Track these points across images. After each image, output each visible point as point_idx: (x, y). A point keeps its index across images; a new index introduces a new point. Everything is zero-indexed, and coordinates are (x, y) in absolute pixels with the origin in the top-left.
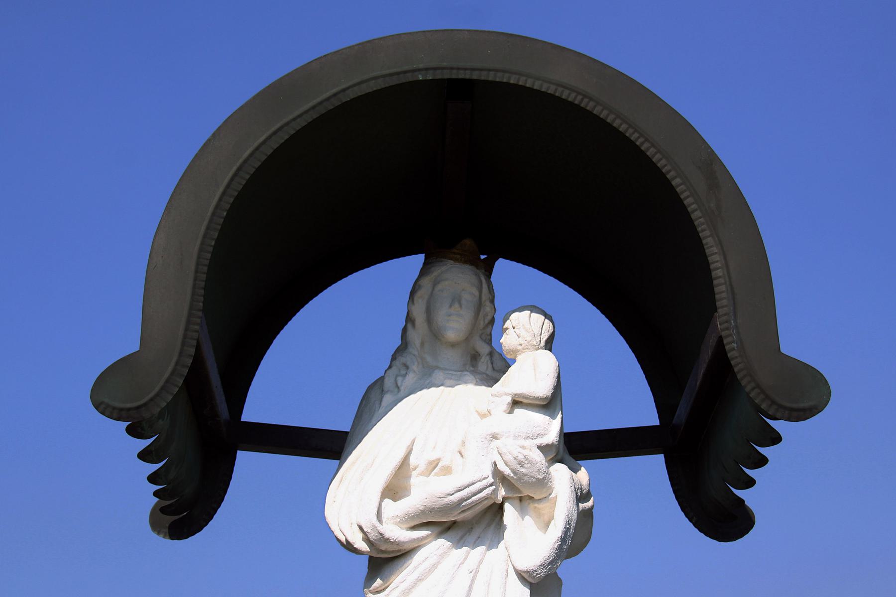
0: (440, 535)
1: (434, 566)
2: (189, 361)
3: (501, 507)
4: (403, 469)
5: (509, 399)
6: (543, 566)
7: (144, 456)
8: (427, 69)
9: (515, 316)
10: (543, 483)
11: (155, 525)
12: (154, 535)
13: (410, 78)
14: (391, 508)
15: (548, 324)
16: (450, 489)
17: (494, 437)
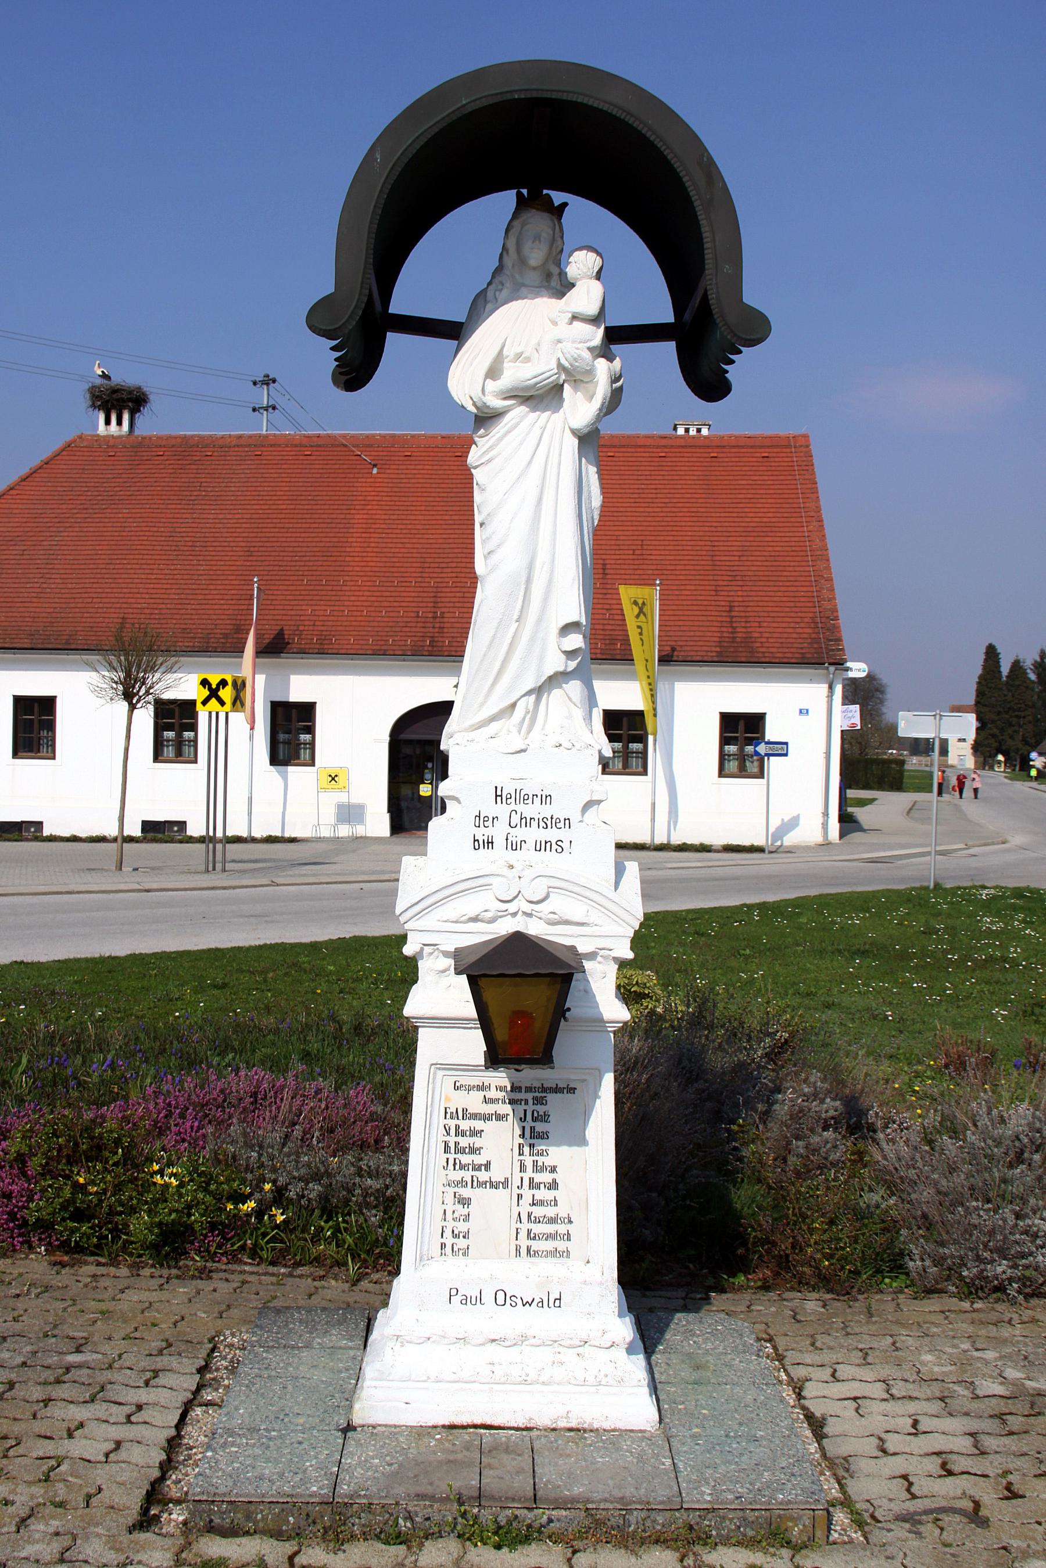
0: (521, 404)
1: (518, 424)
2: (366, 299)
3: (562, 385)
4: (499, 358)
5: (570, 315)
6: (587, 426)
7: (333, 349)
8: (521, 90)
9: (576, 254)
10: (590, 372)
11: (336, 382)
12: (335, 388)
13: (509, 97)
14: (492, 386)
15: (599, 260)
16: (529, 376)
17: (559, 341)
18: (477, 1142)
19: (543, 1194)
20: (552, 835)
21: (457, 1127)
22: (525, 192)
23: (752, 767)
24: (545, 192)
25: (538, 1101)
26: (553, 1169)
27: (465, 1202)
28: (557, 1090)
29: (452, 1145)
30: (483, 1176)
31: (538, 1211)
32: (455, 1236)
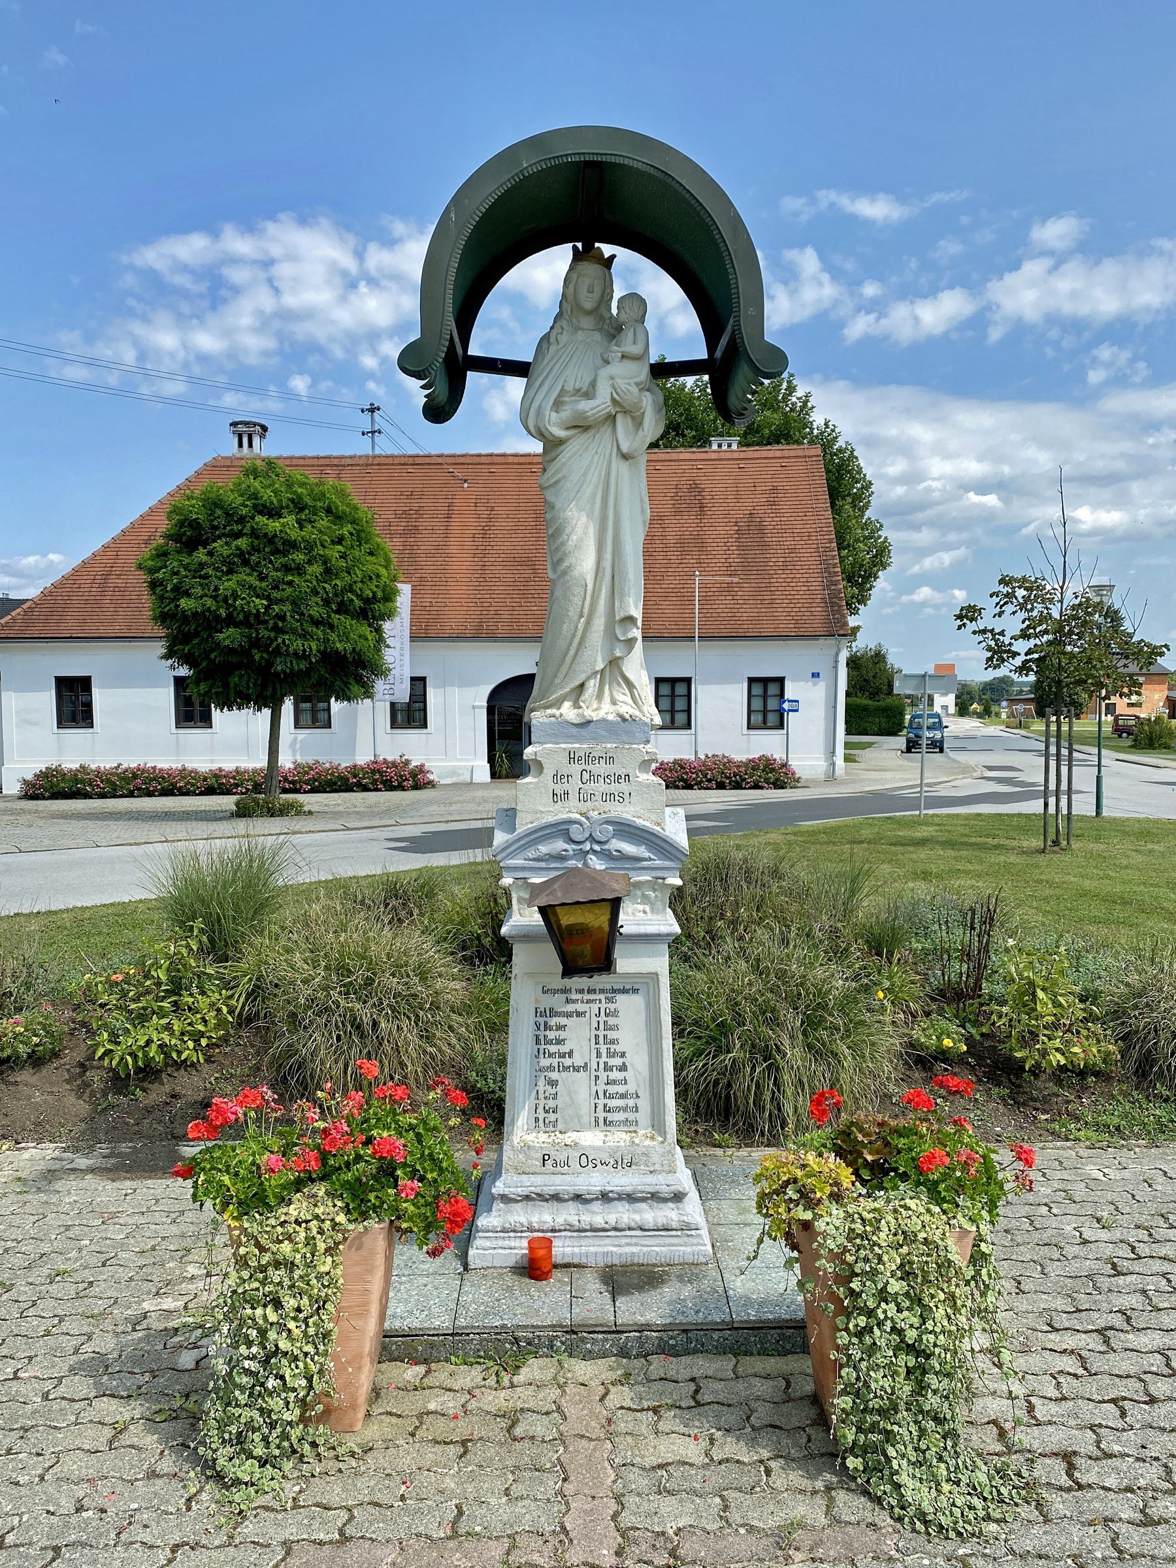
7: (423, 387)
18: (562, 1034)
19: (615, 1075)
20: (614, 788)
21: (546, 1023)
22: (579, 245)
23: (772, 719)
24: (597, 245)
25: (610, 1000)
26: (623, 1055)
27: (553, 1083)
28: (624, 991)
29: (542, 1038)
30: (567, 1062)
31: (612, 1089)
32: (547, 1112)
